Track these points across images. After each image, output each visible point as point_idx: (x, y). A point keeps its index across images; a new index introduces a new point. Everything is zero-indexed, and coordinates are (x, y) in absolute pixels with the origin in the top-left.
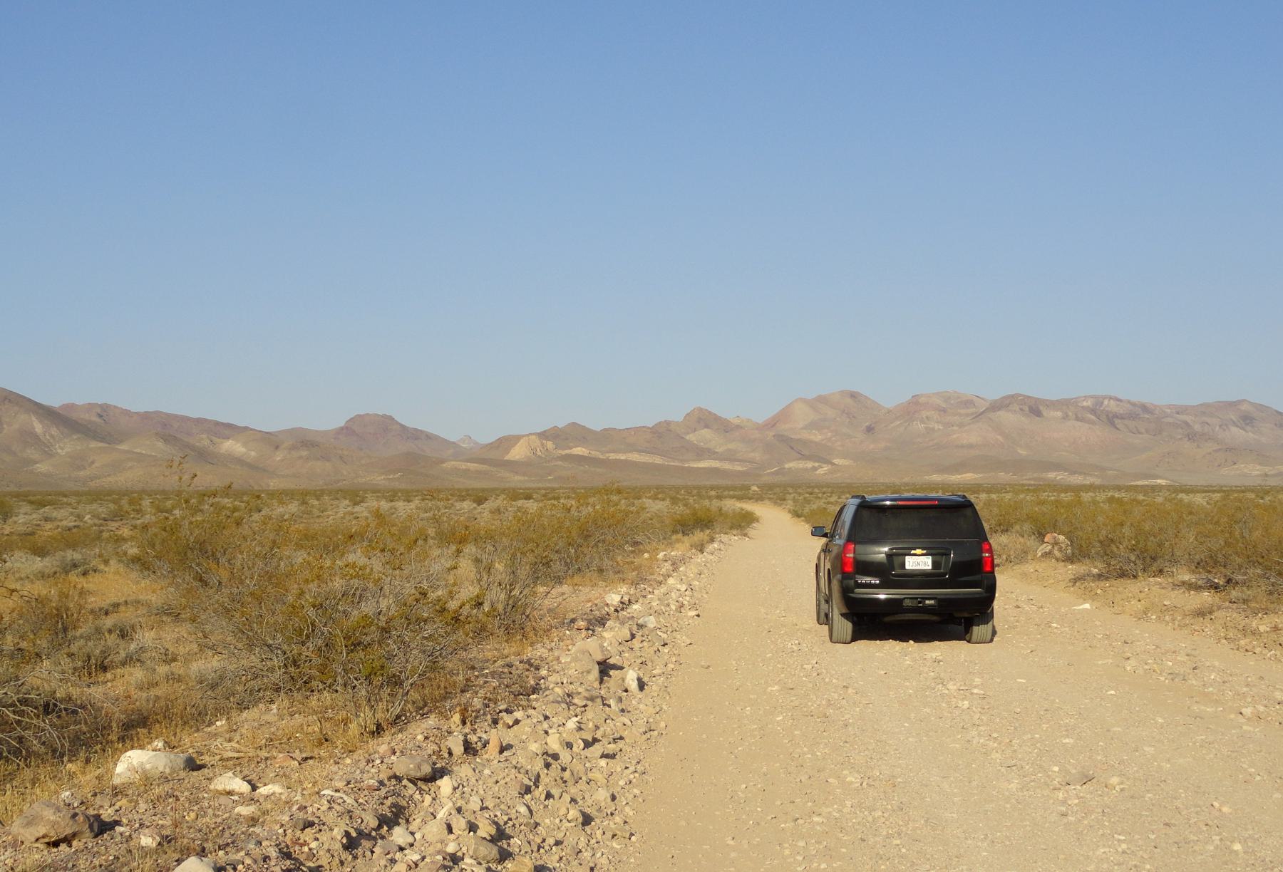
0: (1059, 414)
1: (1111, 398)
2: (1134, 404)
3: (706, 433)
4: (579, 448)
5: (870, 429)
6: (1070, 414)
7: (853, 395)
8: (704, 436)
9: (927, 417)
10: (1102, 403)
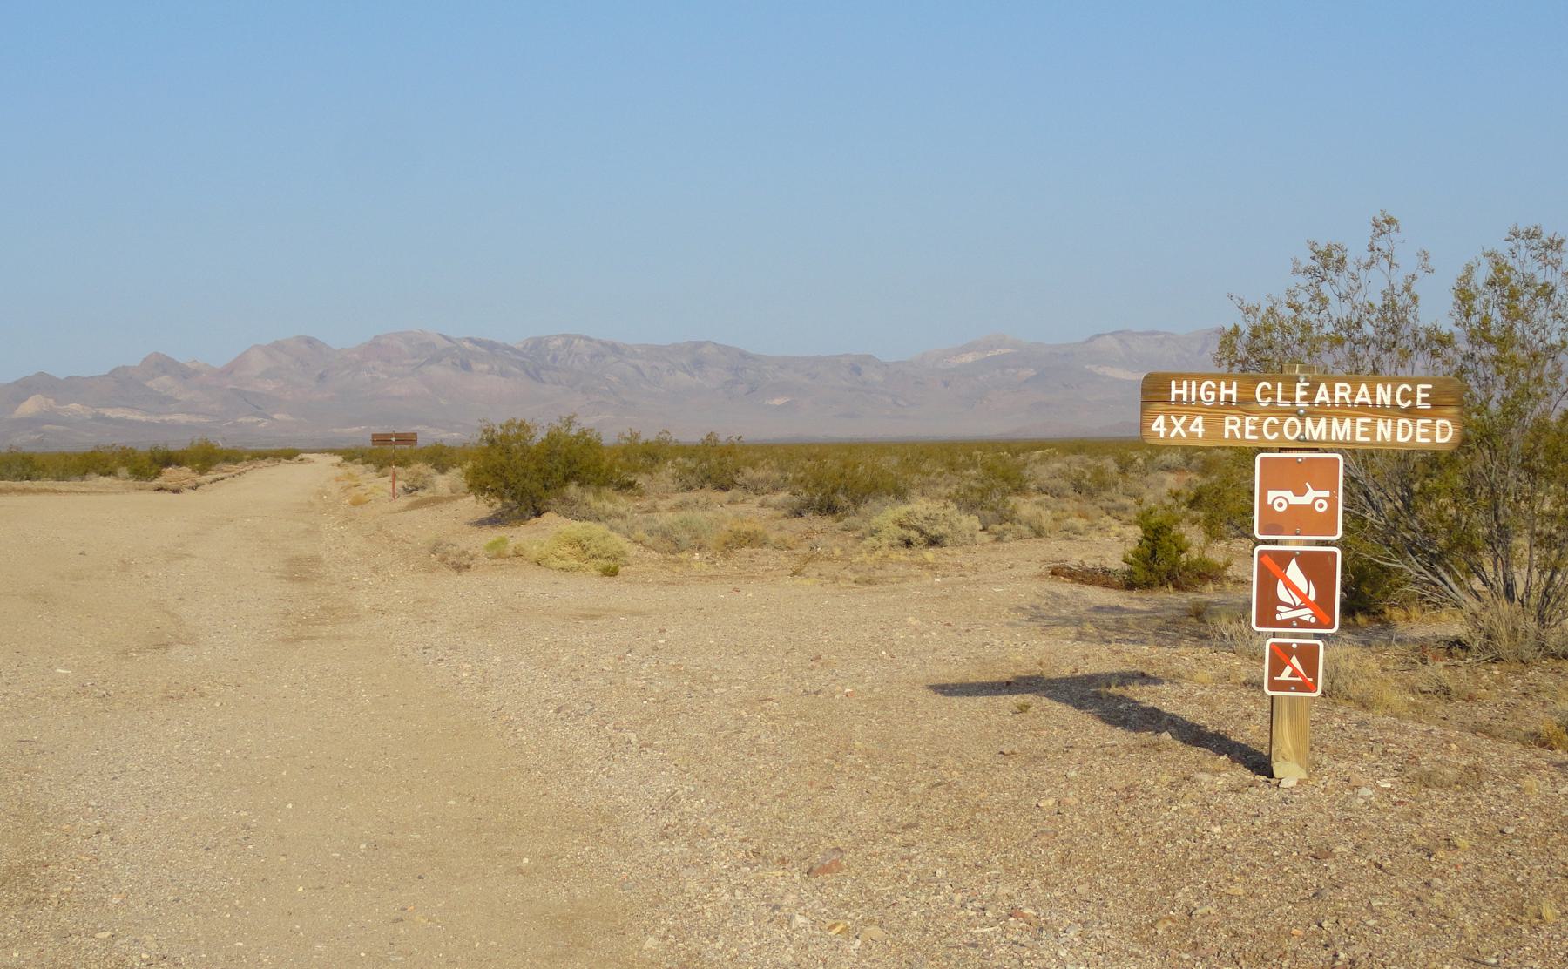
0: (486, 367)
1: (581, 337)
2: (602, 343)
3: (165, 379)
4: (74, 405)
5: (322, 377)
6: (495, 367)
7: (309, 341)
8: (162, 383)
9: (373, 368)
10: (572, 342)
